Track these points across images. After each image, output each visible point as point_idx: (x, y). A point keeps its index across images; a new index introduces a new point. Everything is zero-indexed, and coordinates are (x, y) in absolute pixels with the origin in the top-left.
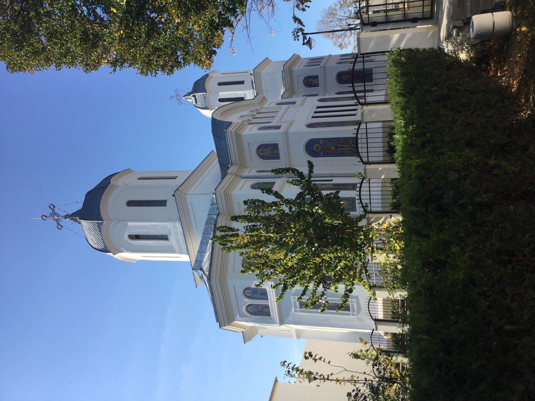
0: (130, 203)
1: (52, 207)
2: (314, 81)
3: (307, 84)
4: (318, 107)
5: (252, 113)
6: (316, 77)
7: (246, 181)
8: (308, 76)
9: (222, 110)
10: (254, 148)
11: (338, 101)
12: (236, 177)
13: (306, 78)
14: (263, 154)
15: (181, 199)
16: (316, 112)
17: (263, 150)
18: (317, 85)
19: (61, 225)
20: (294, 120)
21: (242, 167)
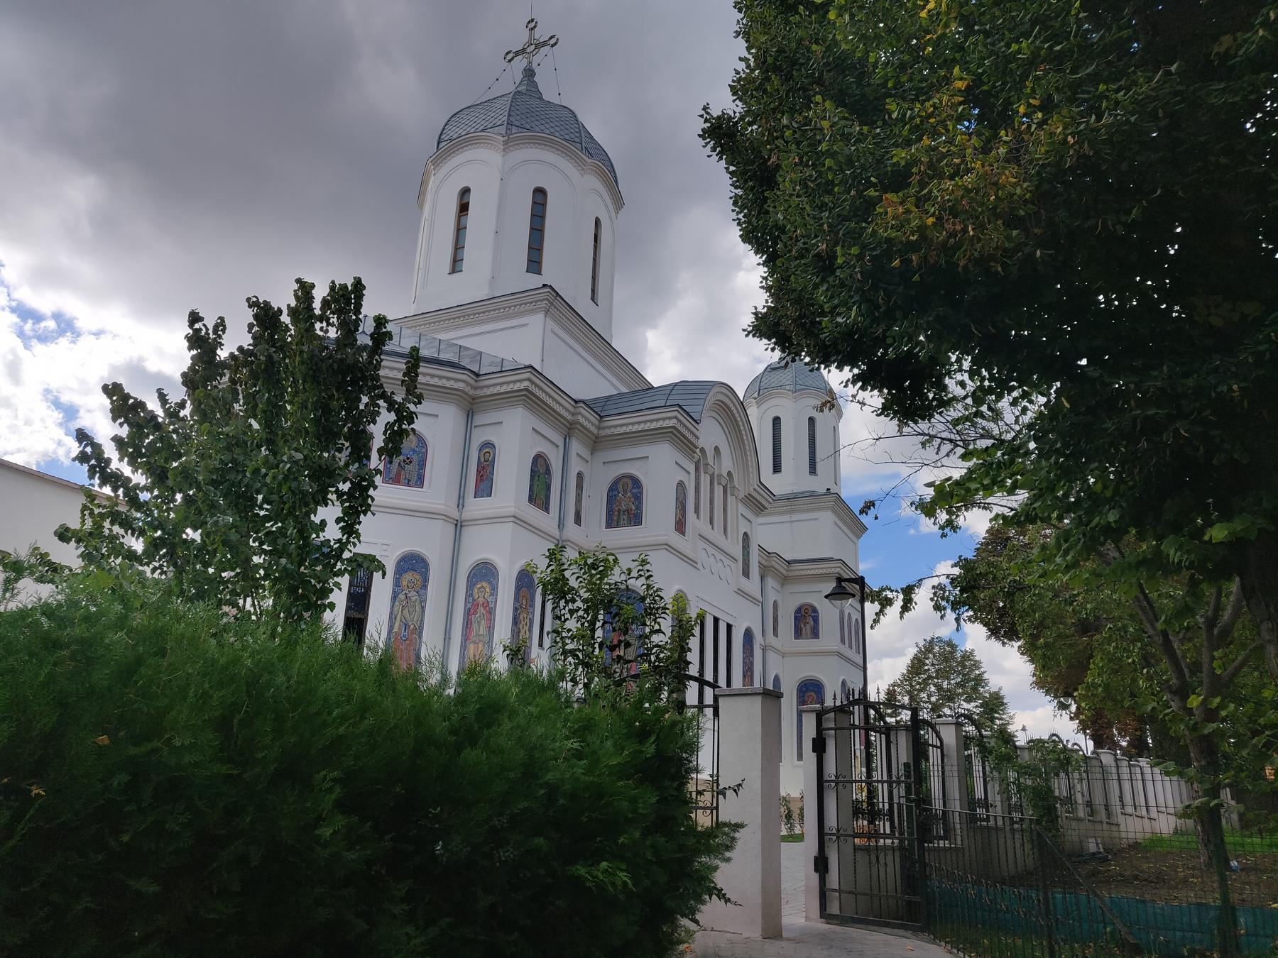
0: (540, 193)
1: (552, 42)
2: (807, 629)
3: (803, 613)
4: (729, 627)
5: (725, 475)
6: (815, 634)
7: (557, 446)
8: (818, 617)
9: (730, 399)
10: (632, 470)
11: (744, 676)
12: (568, 425)
13: (815, 610)
14: (621, 489)
15: (536, 302)
16: (716, 620)
17: (628, 490)
18: (798, 634)
19: (513, 59)
20: (699, 566)
21: (595, 442)
